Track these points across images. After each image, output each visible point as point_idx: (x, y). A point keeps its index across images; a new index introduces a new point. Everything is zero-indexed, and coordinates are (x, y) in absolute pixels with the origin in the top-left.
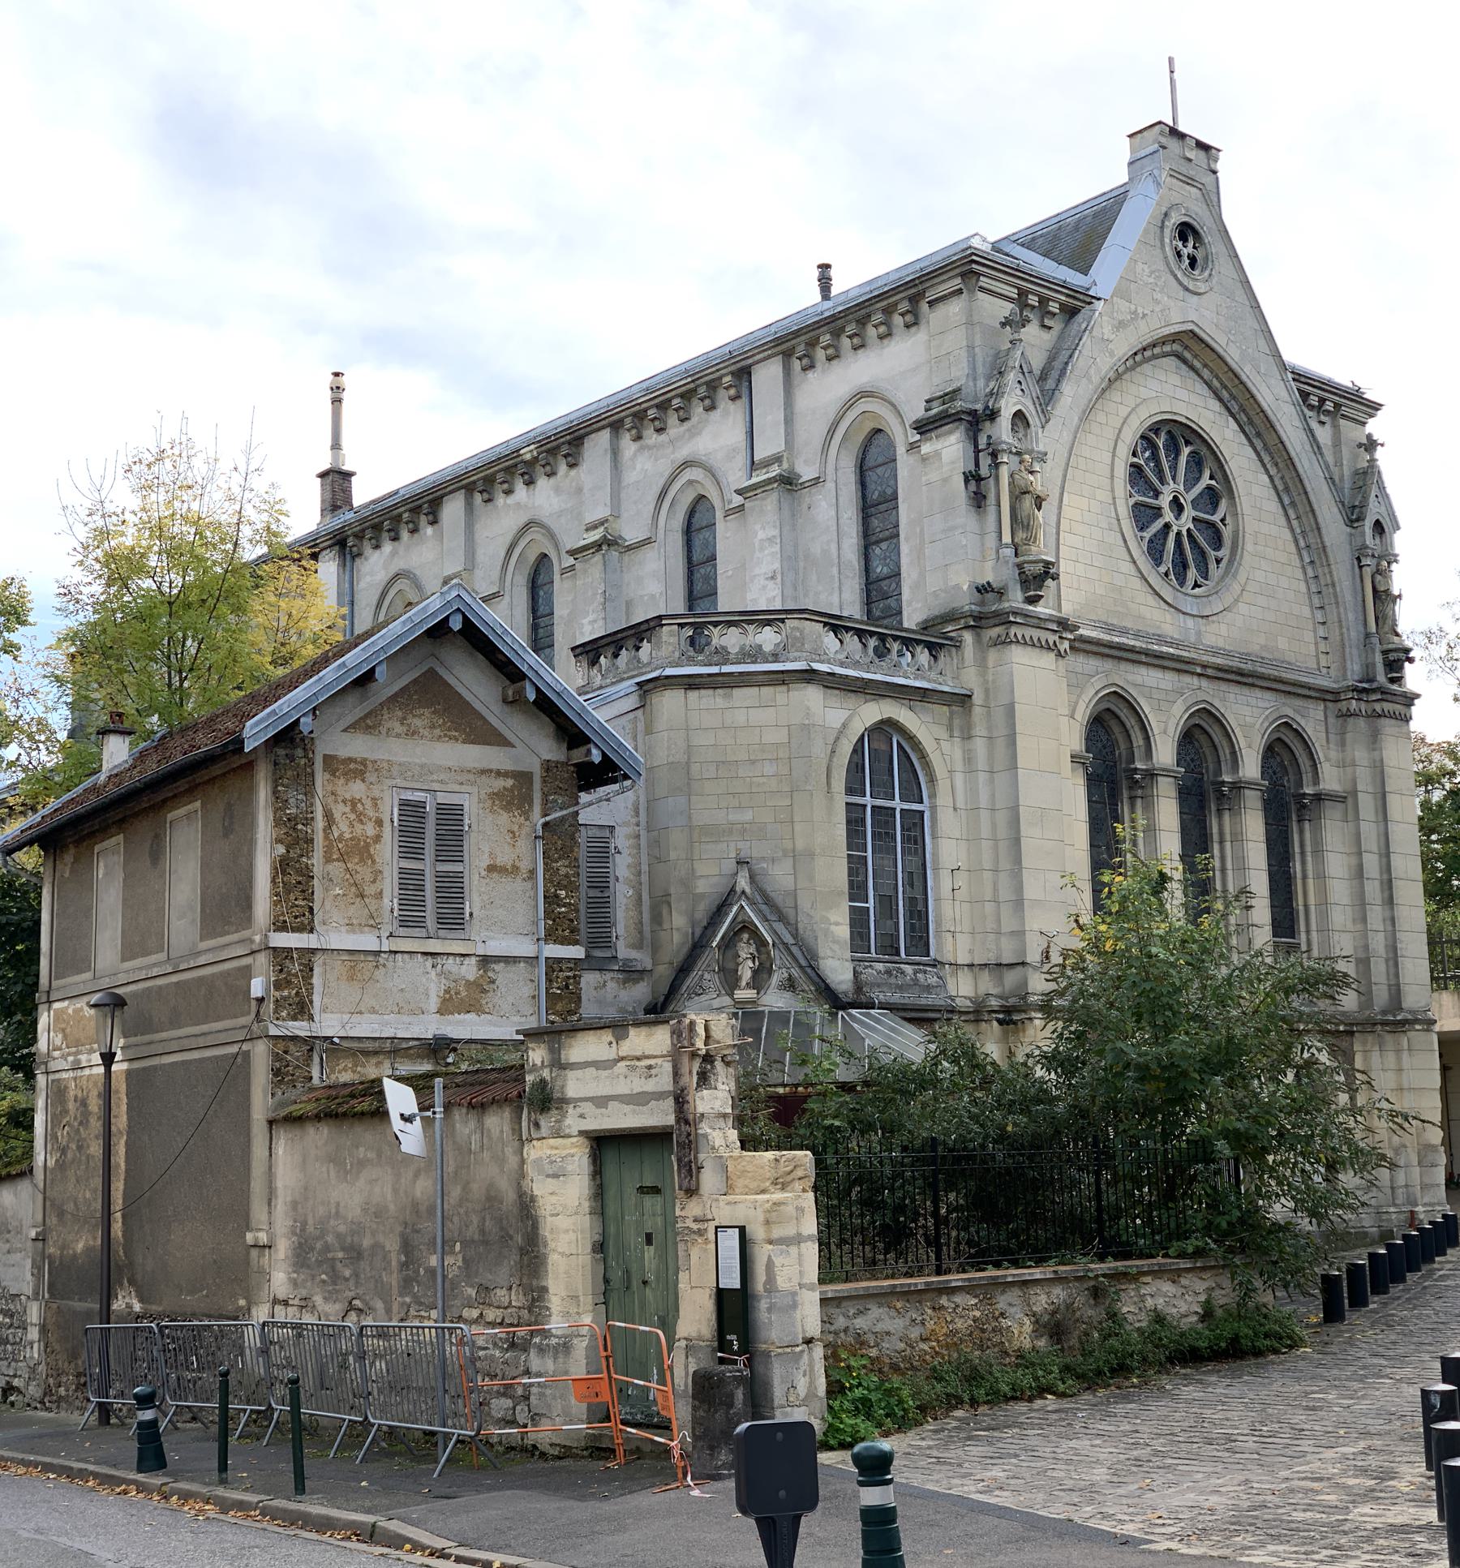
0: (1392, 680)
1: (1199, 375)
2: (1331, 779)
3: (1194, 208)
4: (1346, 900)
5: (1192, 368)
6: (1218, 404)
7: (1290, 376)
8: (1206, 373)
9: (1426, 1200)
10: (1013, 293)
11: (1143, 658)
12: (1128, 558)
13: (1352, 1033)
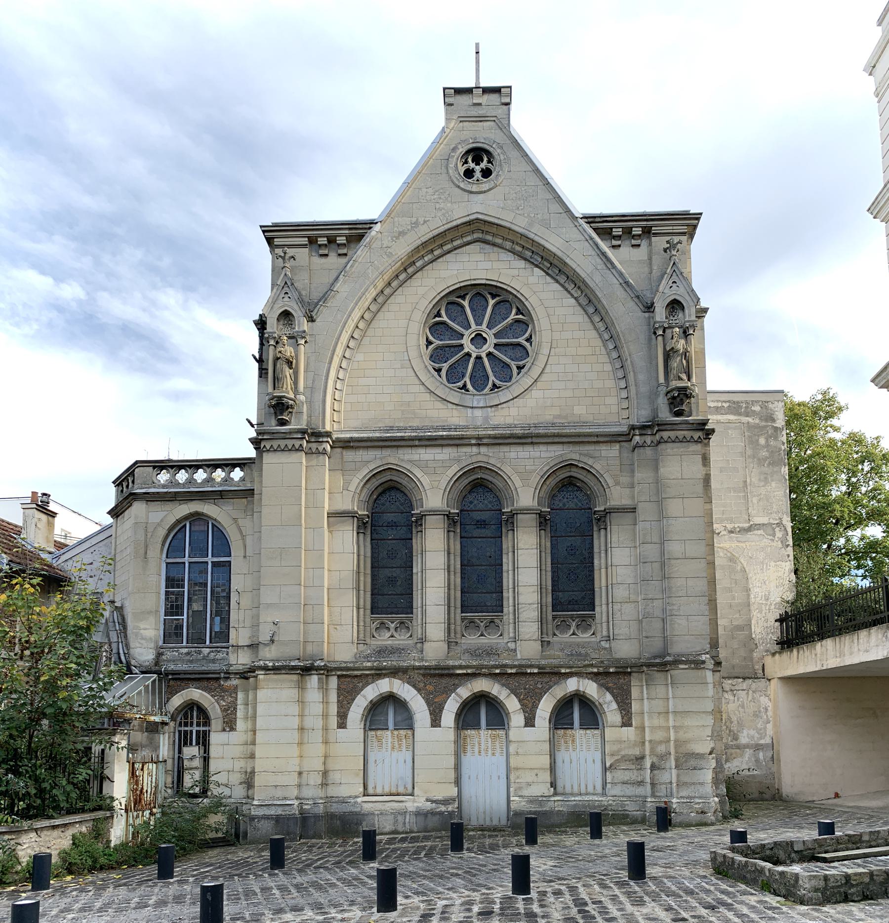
0: (679, 414)
2: (617, 496)
5: (494, 245)
7: (582, 222)
8: (508, 245)
9: (681, 794)
10: (305, 241)
12: (418, 382)
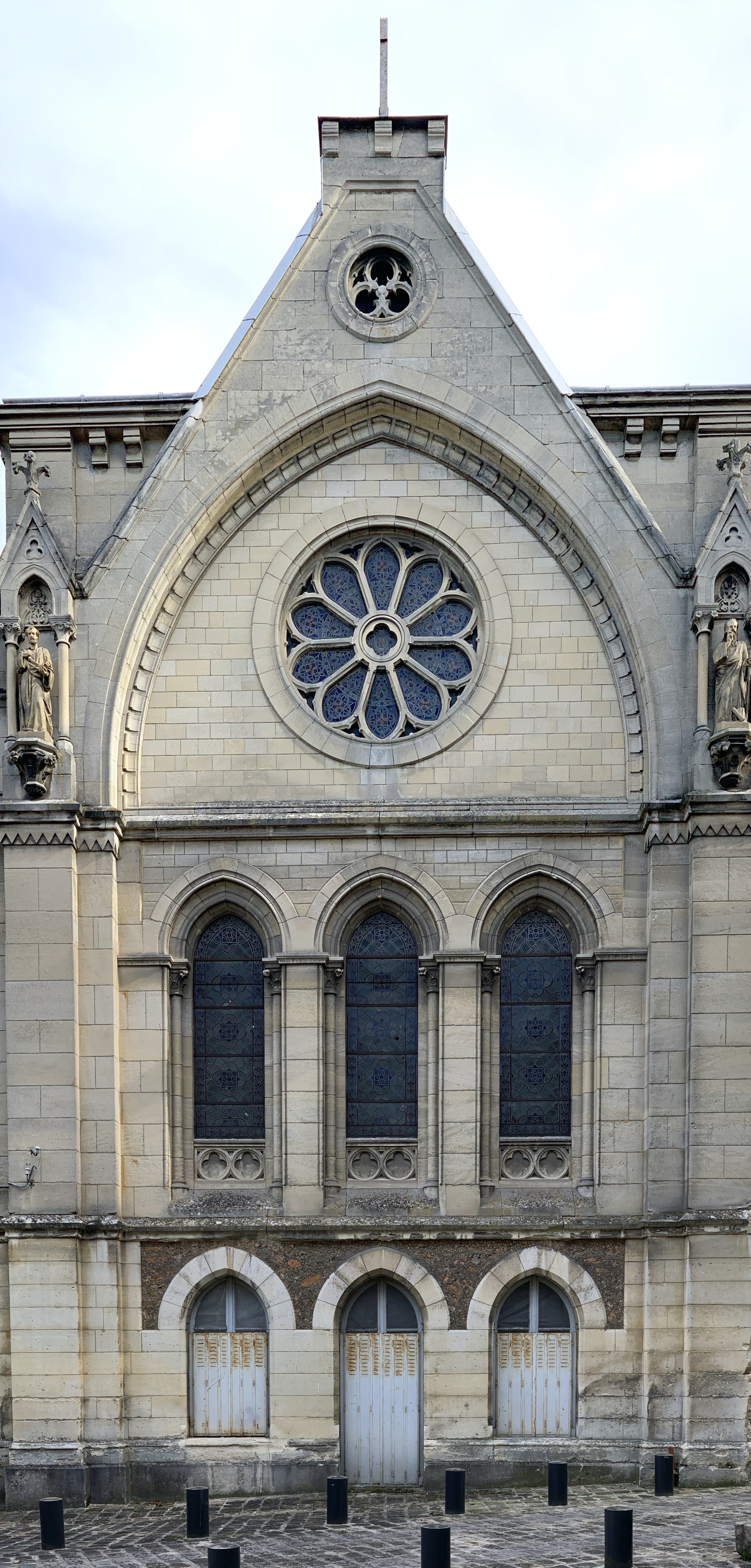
1: (426, 454)
2: (616, 932)
3: (392, 219)
4: (292, 1068)
6: (464, 483)
8: (437, 448)
10: (65, 437)
11: (271, 833)
12: (272, 718)
13: (623, 1241)
